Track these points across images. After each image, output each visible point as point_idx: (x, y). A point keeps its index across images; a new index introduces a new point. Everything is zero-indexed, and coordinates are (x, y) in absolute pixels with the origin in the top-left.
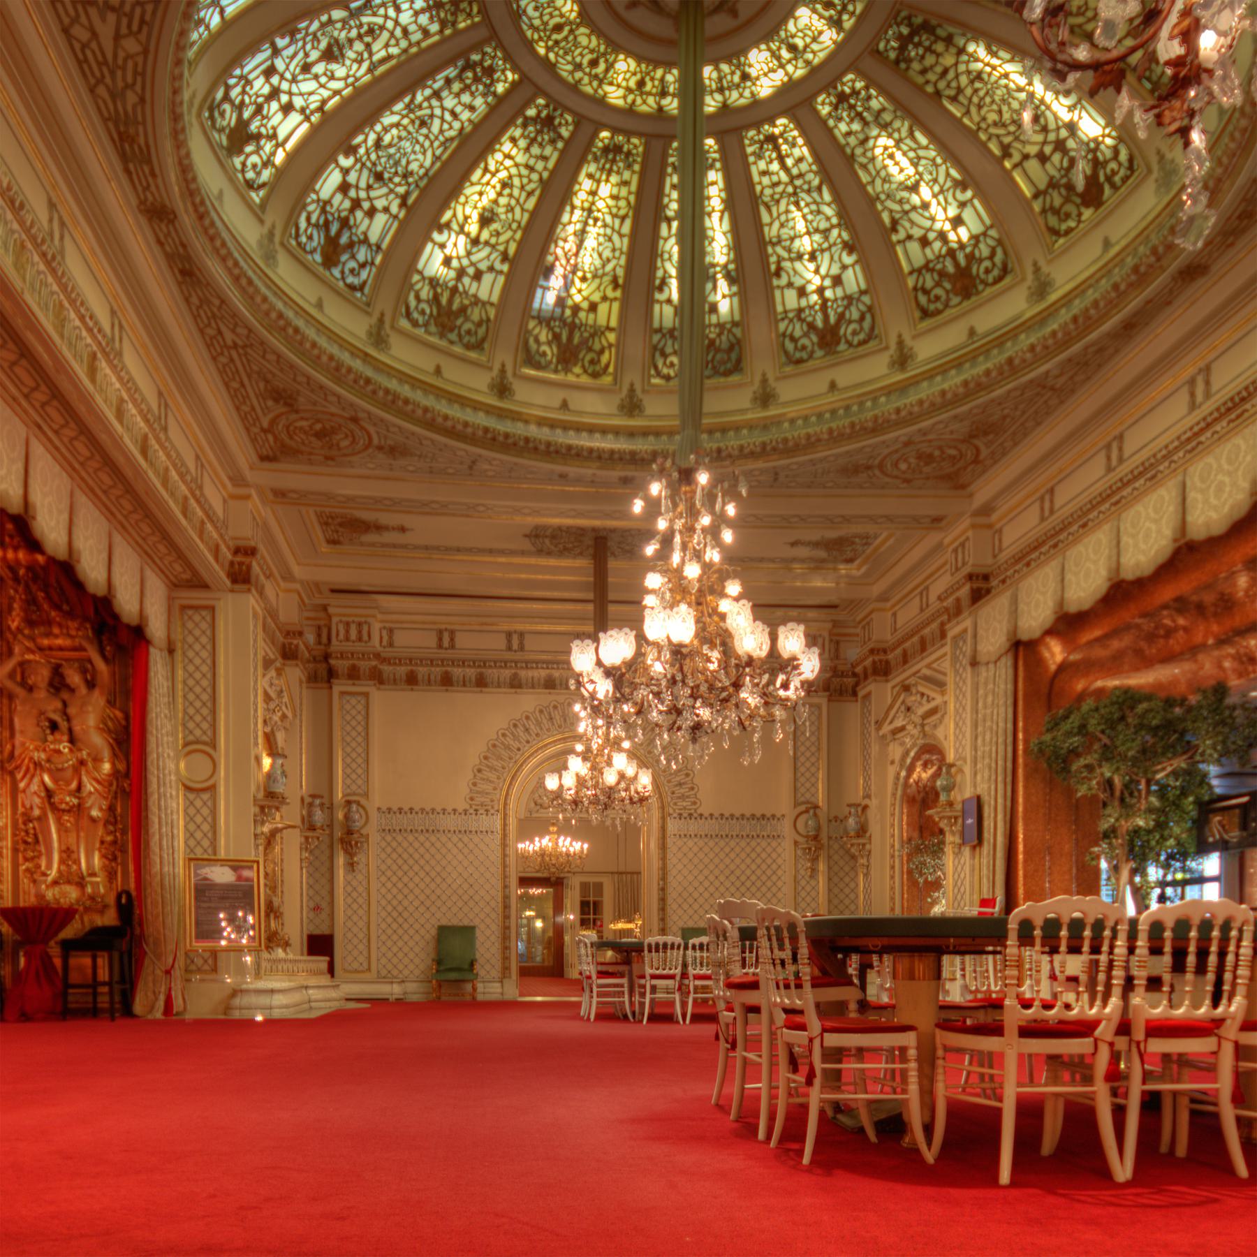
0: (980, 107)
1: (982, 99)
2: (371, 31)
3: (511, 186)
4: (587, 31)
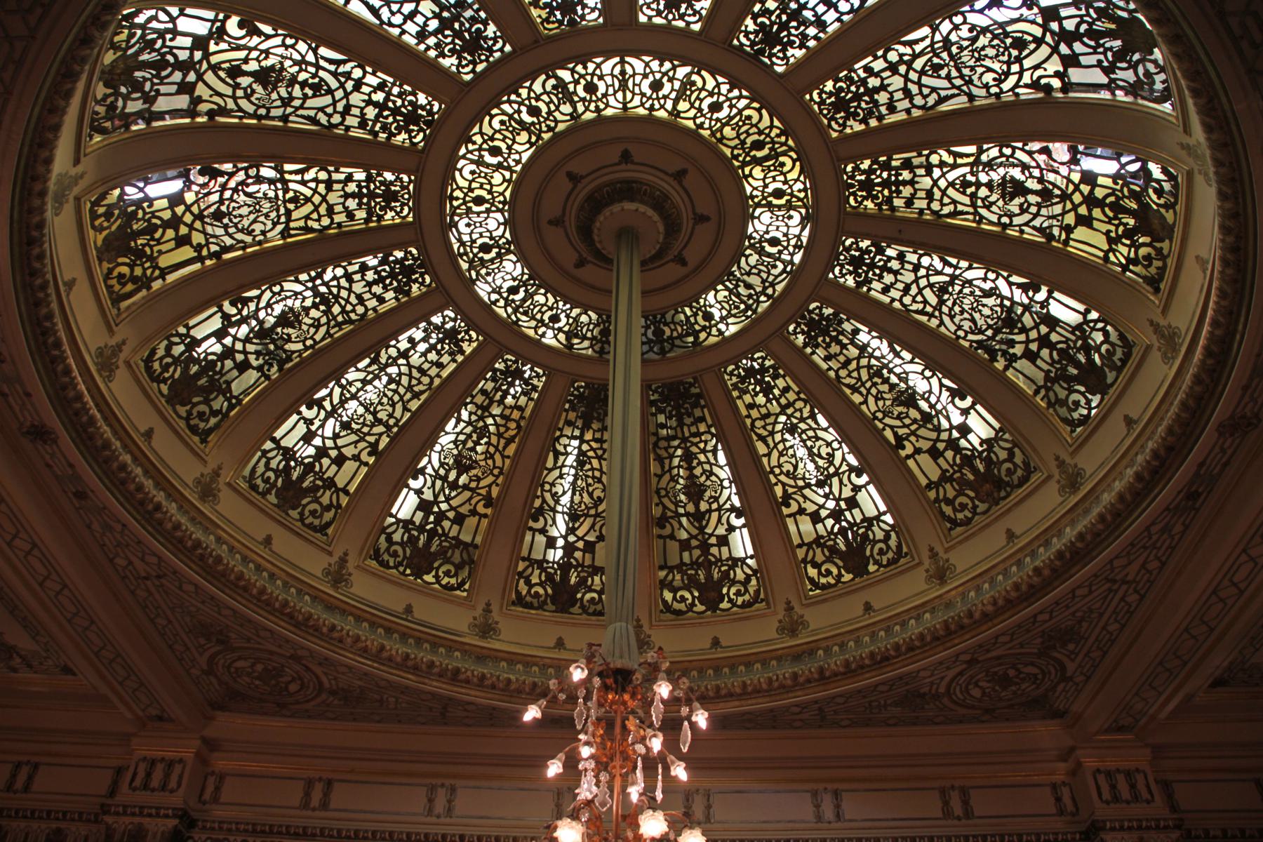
0: (781, 454)
1: (786, 449)
2: (295, 200)
3: (399, 383)
4: (514, 259)
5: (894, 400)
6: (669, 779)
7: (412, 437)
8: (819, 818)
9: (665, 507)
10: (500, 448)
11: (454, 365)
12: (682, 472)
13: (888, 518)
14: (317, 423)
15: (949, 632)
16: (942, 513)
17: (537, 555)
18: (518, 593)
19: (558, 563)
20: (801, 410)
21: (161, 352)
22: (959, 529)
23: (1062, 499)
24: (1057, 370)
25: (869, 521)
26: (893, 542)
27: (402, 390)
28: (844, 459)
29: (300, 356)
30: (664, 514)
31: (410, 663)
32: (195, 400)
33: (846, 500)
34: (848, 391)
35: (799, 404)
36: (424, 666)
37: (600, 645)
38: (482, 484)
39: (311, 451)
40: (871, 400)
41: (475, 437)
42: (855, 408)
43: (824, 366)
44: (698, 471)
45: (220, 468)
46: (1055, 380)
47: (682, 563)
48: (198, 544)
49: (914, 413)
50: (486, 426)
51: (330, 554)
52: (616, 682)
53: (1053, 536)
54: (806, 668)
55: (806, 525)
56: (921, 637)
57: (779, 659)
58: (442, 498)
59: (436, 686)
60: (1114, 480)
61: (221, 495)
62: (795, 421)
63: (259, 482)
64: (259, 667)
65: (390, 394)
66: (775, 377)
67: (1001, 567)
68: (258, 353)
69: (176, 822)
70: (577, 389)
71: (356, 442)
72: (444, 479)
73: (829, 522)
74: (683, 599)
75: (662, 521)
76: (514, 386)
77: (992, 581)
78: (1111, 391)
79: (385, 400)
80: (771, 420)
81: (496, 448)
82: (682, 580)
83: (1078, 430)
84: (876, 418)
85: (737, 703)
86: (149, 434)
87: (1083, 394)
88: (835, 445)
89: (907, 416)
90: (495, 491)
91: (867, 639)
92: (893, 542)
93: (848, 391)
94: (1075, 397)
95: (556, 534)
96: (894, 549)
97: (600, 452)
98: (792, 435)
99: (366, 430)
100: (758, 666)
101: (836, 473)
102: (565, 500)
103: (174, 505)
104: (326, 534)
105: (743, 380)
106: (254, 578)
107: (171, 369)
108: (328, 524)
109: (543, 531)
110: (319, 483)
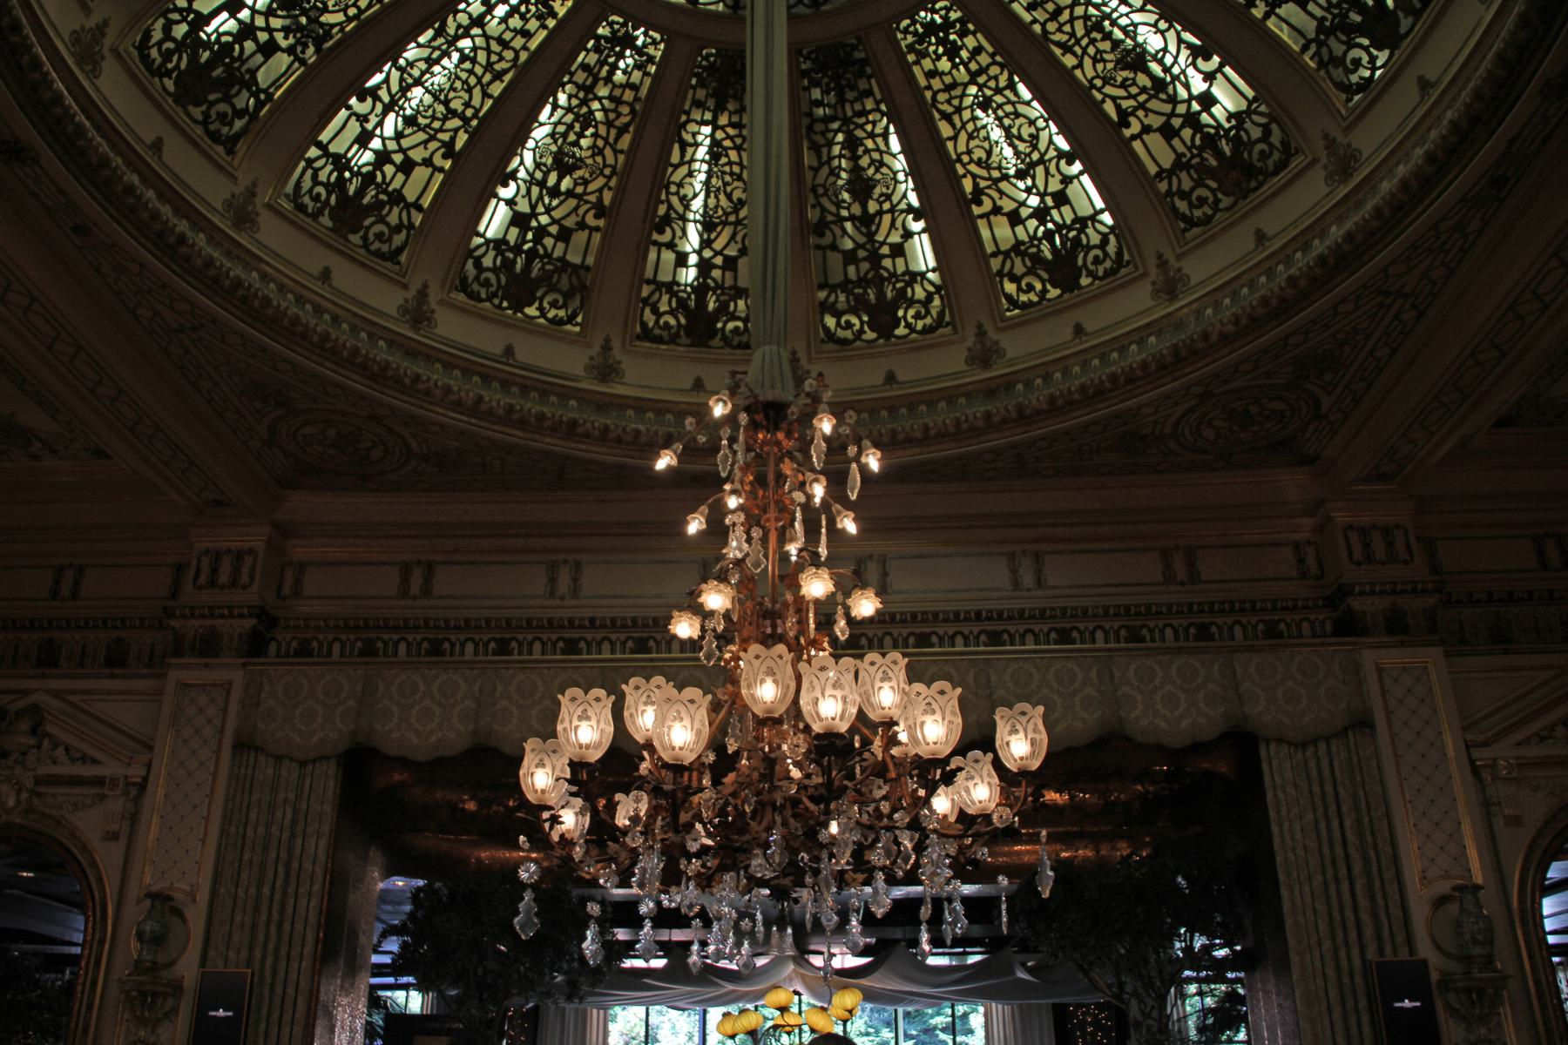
0: (971, 137)
1: (977, 130)
3: (474, 61)
5: (1118, 62)
6: (835, 534)
7: (499, 132)
8: (1016, 585)
9: (824, 210)
10: (611, 140)
11: (545, 33)
12: (844, 163)
13: (1107, 218)
14: (373, 120)
15: (1179, 359)
16: (1175, 209)
17: (665, 277)
18: (644, 325)
19: (691, 285)
20: (996, 78)
21: (157, 35)
22: (1195, 230)
23: (1328, 190)
24: (1335, 17)
25: (1081, 222)
26: (1112, 248)
27: (479, 70)
28: (1051, 142)
29: (342, 30)
30: (822, 218)
31: (515, 416)
32: (212, 97)
33: (1053, 195)
34: (1058, 51)
35: (994, 70)
36: (533, 420)
37: (745, 373)
38: (591, 188)
39: (368, 156)
40: (1087, 62)
41: (577, 127)
42: (1068, 73)
43: (1027, 17)
44: (864, 162)
45: (255, 185)
46: (1330, 32)
47: (847, 281)
48: (238, 283)
49: (1143, 80)
50: (591, 112)
51: (405, 287)
52: (767, 417)
53: (1314, 238)
54: (1001, 406)
55: (1003, 231)
56: (1144, 365)
57: (968, 395)
58: (541, 209)
59: (548, 443)
60: (1398, 164)
61: (260, 219)
62: (989, 93)
63: (306, 199)
64: (332, 433)
65: (464, 75)
66: (963, 34)
67: (1246, 278)
68: (286, 30)
69: (253, 622)
70: (706, 58)
71: (425, 143)
72: (542, 184)
73: (1033, 223)
74: (849, 325)
75: (820, 228)
76: (624, 57)
77: (1235, 295)
78: (1405, 44)
79: (458, 84)
80: (958, 92)
81: (606, 140)
82: (848, 301)
83: (1356, 98)
84: (1093, 86)
85: (917, 450)
86: (157, 146)
87: (1366, 49)
88: (1041, 123)
89: (1134, 83)
90: (607, 197)
91: (1077, 369)
92: (1112, 248)
93: (1058, 51)
94: (1356, 53)
95: (688, 249)
96: (1113, 256)
97: (738, 141)
98: (985, 111)
99: (437, 125)
100: (942, 405)
101: (1041, 161)
102: (697, 204)
103: (202, 236)
104: (399, 263)
105: (921, 39)
106: (313, 322)
107: (175, 58)
108: (400, 250)
109: (671, 246)
110: (383, 197)
